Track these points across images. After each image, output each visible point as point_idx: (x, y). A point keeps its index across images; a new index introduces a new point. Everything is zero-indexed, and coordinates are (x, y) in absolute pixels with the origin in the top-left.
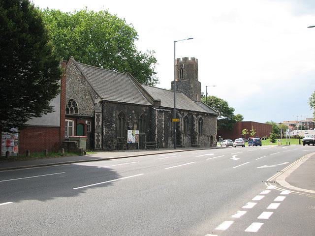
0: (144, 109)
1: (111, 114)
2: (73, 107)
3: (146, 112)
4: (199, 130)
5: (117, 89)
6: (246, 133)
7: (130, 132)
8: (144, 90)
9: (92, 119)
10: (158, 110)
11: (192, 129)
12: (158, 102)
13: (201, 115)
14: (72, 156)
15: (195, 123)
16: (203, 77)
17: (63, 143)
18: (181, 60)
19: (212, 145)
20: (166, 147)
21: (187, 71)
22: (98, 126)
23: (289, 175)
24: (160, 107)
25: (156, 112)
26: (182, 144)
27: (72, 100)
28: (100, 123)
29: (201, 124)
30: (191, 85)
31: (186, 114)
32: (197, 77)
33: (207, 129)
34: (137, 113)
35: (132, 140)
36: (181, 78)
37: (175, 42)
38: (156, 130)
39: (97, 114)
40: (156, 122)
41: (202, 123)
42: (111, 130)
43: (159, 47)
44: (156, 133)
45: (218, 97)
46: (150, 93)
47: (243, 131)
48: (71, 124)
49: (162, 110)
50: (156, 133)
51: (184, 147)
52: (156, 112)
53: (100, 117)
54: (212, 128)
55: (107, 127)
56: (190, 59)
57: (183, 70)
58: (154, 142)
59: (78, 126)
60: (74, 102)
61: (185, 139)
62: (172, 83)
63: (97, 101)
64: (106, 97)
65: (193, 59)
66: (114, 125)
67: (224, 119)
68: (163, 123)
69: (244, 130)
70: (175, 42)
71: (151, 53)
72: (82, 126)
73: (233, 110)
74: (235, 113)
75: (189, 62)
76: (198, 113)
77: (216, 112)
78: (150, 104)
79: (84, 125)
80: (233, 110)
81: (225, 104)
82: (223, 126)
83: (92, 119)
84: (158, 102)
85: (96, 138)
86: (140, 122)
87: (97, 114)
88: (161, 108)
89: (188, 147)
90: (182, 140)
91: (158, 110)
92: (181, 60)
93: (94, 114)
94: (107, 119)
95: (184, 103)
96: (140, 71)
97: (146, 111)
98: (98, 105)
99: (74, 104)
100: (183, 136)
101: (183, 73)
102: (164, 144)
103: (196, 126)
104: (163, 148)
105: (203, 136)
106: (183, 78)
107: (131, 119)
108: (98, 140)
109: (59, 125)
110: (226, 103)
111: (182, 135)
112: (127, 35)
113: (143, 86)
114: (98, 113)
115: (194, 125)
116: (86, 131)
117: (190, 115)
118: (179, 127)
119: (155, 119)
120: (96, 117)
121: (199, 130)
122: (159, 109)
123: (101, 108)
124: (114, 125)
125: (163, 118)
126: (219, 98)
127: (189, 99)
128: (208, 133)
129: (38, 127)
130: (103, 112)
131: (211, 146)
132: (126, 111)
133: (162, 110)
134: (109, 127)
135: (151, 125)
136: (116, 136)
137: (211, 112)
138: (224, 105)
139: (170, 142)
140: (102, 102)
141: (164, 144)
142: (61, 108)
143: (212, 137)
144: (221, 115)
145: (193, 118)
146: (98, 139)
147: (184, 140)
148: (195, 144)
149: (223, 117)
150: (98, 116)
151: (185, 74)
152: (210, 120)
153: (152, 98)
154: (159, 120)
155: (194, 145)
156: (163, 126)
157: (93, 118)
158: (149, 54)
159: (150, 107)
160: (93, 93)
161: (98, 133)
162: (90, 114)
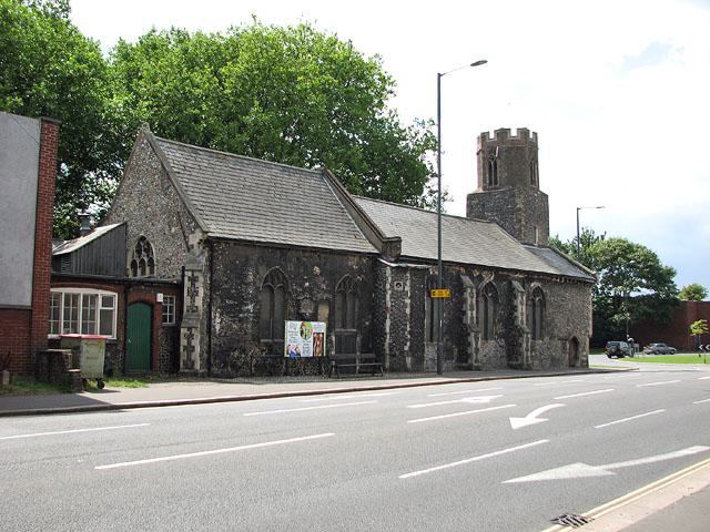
0: (353, 263)
1: (241, 277)
2: (146, 260)
3: (360, 272)
4: (534, 322)
5: (291, 211)
6: (701, 331)
7: (293, 327)
8: (360, 212)
9: (176, 289)
10: (393, 265)
11: (509, 319)
12: (395, 243)
13: (540, 280)
14: (35, 393)
15: (518, 302)
16: (551, 177)
17: (40, 354)
18: (492, 136)
19: (576, 365)
20: (418, 369)
21: (510, 163)
22: (194, 309)
23: (651, 513)
24: (399, 258)
25: (388, 271)
26: (472, 361)
27: (143, 239)
28: (199, 301)
29: (538, 303)
30: (517, 200)
31: (489, 278)
32: (534, 179)
33: (560, 320)
34: (330, 276)
35: (301, 350)
36: (490, 183)
37: (440, 75)
38: (388, 322)
39: (190, 274)
40: (388, 297)
41: (543, 304)
42: (241, 320)
43: (443, 105)
44: (388, 330)
45: (634, 240)
46: (375, 221)
47: (692, 326)
48: (107, 301)
49: (403, 265)
50: (388, 330)
51: (478, 369)
52: (388, 271)
53: (197, 285)
54: (578, 314)
55: (225, 310)
56: (514, 133)
57: (495, 163)
58: (351, 356)
59: (131, 309)
60: (148, 244)
61: (485, 348)
62: (470, 197)
63: (194, 239)
64: (216, 230)
65: (524, 132)
66: (250, 307)
67: (648, 296)
68: (408, 301)
69: (696, 323)
70: (440, 75)
71: (427, 125)
72: (147, 309)
73: (671, 273)
74: (681, 283)
75: (514, 140)
76: (530, 276)
77: (588, 273)
78: (371, 249)
79: (152, 305)
80: (671, 273)
81: (650, 258)
82: (645, 313)
83: (176, 289)
84: (395, 243)
85: (184, 342)
86: (339, 299)
87: (190, 274)
88: (402, 261)
89: (500, 367)
90: (472, 350)
91: (393, 265)
92: (492, 136)
93: (183, 276)
94: (229, 290)
95: (498, 250)
96: (398, 171)
97: (360, 268)
98: (197, 250)
99: (149, 250)
100: (476, 339)
101: (496, 168)
102: (409, 360)
103: (522, 311)
104: (407, 371)
105: (547, 339)
106: (496, 184)
107: (310, 290)
108: (190, 349)
109: (27, 301)
110: (654, 256)
111: (473, 334)
112: (354, 84)
113: (358, 201)
114: (193, 271)
115: (514, 308)
116: (158, 322)
117: (501, 281)
118: (464, 313)
119: (385, 291)
120: (187, 283)
121: (534, 322)
122: (395, 262)
123: (203, 260)
124: (250, 307)
125: (407, 288)
126: (635, 243)
127: (510, 239)
128: (562, 326)
129: (19, 310)
130: (211, 268)
131: (572, 366)
132: (291, 267)
133: (403, 265)
134: (233, 311)
135: (374, 309)
136: (256, 339)
137: (572, 273)
138: (646, 260)
139: (430, 352)
140: (210, 243)
141: (409, 360)
142: (35, 253)
143: (575, 341)
144: (642, 285)
145: (511, 289)
146: (189, 343)
147: (477, 350)
148: (466, 361)
149: (645, 292)
150: (193, 280)
151: (502, 174)
152: (570, 297)
153: (379, 234)
154: (397, 293)
155: (513, 363)
156: (408, 311)
157: (180, 286)
158: (420, 128)
159: (373, 258)
160: (185, 218)
161: (189, 329)
162: (173, 275)
